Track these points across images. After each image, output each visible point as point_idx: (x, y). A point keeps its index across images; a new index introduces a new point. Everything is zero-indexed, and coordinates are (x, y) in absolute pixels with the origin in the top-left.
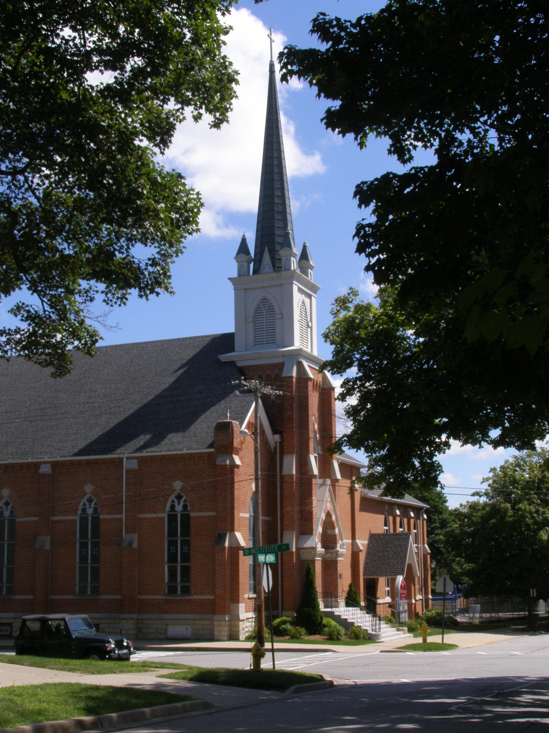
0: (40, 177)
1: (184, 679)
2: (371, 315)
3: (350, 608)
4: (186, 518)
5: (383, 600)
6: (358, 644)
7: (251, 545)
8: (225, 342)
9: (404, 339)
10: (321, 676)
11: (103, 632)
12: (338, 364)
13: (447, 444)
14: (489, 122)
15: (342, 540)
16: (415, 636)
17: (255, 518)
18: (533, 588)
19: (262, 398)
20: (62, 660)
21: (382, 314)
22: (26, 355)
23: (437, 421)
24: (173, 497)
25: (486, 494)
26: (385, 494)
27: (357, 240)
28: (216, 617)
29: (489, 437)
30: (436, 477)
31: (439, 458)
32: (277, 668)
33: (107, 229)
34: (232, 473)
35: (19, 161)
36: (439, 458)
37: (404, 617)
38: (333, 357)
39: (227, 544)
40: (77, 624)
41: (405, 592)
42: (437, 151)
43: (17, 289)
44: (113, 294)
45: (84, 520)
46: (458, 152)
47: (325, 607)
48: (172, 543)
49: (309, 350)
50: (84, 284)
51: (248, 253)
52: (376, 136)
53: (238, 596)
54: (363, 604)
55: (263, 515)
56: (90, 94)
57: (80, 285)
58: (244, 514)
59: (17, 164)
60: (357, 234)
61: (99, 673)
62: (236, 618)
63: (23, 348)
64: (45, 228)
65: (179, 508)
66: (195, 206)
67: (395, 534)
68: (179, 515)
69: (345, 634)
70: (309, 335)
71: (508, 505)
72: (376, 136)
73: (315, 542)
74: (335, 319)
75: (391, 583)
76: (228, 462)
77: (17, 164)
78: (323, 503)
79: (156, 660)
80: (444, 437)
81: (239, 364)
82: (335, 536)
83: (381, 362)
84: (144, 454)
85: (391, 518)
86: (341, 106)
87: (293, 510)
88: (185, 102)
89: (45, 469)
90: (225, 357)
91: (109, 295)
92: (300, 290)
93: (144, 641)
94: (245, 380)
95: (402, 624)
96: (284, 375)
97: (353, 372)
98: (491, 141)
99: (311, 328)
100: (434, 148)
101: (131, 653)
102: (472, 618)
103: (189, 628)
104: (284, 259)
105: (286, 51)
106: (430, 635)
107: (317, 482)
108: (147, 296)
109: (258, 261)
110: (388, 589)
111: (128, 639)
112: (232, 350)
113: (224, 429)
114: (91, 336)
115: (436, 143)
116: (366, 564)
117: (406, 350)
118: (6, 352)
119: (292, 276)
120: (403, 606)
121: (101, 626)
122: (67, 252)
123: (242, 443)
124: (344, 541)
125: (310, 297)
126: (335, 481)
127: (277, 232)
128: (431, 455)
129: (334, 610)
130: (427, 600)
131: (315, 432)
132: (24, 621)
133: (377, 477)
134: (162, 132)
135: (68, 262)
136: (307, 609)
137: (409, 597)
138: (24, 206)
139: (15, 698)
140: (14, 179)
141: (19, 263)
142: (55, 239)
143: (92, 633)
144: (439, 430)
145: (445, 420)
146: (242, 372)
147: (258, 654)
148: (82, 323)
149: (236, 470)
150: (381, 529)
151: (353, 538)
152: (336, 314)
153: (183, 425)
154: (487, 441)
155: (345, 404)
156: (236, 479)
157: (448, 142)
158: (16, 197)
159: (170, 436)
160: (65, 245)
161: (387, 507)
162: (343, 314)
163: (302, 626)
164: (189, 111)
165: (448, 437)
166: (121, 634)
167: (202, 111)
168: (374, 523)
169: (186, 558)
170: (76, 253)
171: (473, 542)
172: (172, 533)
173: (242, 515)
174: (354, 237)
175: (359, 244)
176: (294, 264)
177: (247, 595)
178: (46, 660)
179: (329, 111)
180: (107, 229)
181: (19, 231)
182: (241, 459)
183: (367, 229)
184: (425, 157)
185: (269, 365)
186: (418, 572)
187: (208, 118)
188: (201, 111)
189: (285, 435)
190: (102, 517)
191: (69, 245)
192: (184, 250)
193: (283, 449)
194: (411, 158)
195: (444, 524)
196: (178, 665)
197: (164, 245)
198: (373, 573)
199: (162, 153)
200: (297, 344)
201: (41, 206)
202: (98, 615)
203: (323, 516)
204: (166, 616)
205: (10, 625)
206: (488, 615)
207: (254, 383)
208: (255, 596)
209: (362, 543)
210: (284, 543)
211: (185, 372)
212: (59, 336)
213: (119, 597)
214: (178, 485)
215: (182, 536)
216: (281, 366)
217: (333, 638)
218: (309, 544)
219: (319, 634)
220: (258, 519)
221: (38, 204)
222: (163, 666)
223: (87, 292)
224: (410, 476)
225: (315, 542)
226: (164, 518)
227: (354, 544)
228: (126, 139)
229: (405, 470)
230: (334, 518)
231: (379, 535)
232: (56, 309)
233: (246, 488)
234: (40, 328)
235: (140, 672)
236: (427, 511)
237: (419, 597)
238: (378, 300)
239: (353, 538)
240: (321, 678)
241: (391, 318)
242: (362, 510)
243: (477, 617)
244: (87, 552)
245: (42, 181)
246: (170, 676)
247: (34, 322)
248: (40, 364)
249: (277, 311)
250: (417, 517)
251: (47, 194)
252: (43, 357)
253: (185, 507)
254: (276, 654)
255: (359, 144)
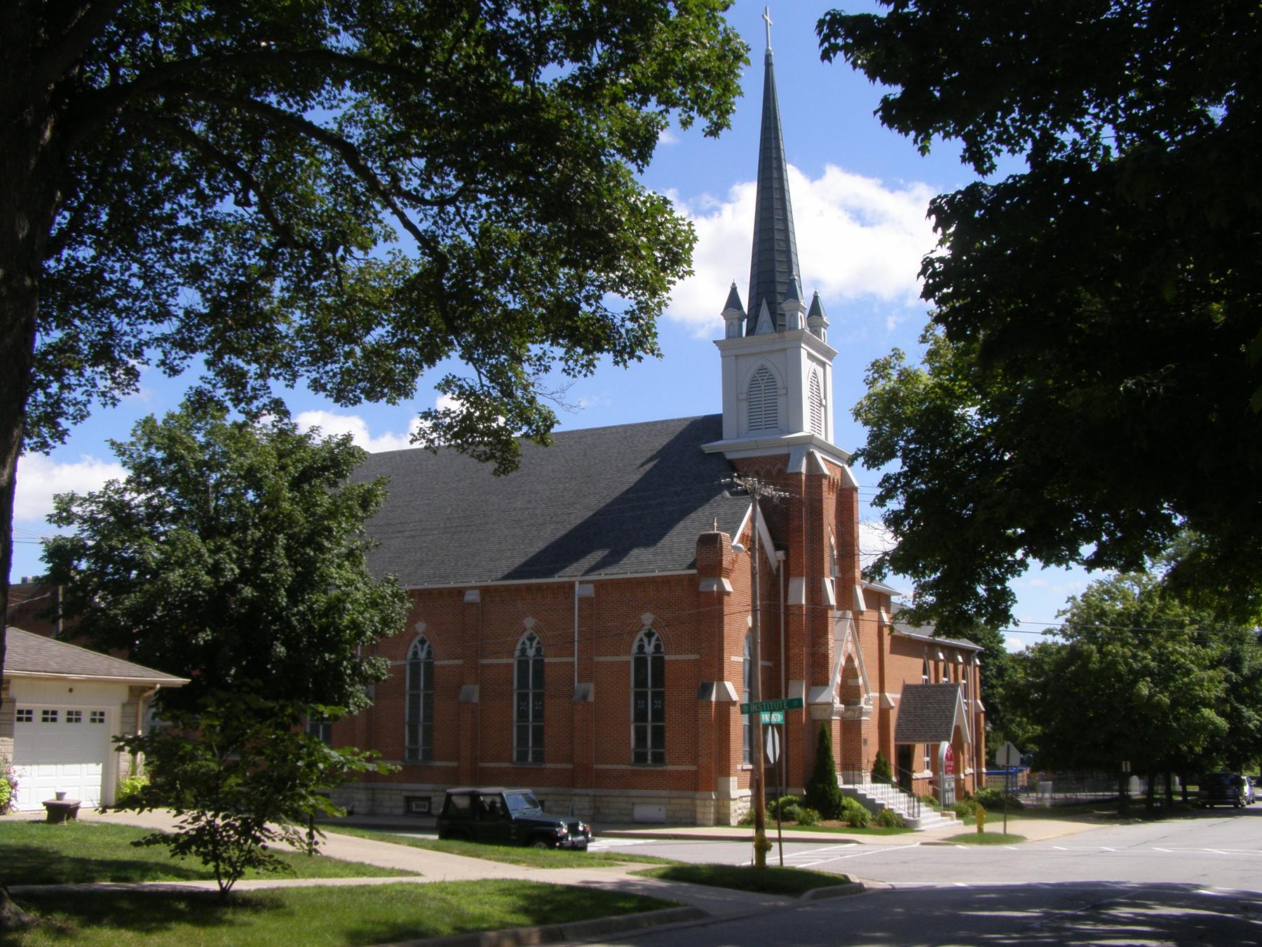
0: (476, 206)
1: (652, 876)
2: (922, 387)
3: (879, 785)
4: (659, 662)
5: (922, 773)
6: (891, 834)
7: (746, 701)
8: (709, 426)
9: (962, 418)
10: (846, 877)
11: (549, 812)
12: (874, 457)
13: (1023, 564)
14: (1101, 115)
15: (867, 692)
16: (966, 823)
17: (752, 663)
18: (1126, 760)
19: (760, 502)
20: (502, 848)
21: (935, 386)
22: (458, 446)
23: (1010, 531)
24: (641, 635)
25: (1063, 632)
26: (936, 633)
27: (922, 280)
28: (699, 794)
29: (1079, 554)
30: (1006, 610)
31: (1012, 583)
32: (786, 864)
33: (564, 274)
34: (721, 602)
35: (449, 186)
36: (1012, 583)
37: (951, 797)
38: (870, 443)
39: (713, 698)
40: (518, 801)
41: (952, 763)
42: (1029, 158)
43: (444, 358)
44: (576, 361)
45: (523, 664)
46: (1058, 157)
47: (845, 783)
48: (640, 696)
49: (823, 438)
50: (535, 349)
51: (740, 307)
52: (944, 138)
53: (729, 767)
54: (894, 779)
55: (763, 659)
56: (543, 95)
57: (529, 350)
58: (736, 658)
59: (445, 191)
60: (923, 272)
61: (551, 866)
62: (725, 797)
63: (455, 436)
64: (482, 275)
65: (649, 649)
66: (687, 239)
67: (938, 686)
68: (649, 659)
69: (872, 820)
70: (828, 413)
71: (1093, 647)
72: (944, 138)
73: (832, 695)
74: (871, 391)
75: (933, 751)
76: (715, 588)
77: (445, 191)
78: (843, 643)
79: (615, 850)
80: (1019, 554)
81: (729, 456)
82: (858, 687)
83: (933, 452)
84: (603, 575)
85: (932, 663)
86: (903, 93)
87: (802, 653)
88: (669, 102)
89: (473, 596)
90: (708, 447)
91: (571, 362)
92: (810, 356)
93: (604, 823)
94: (739, 477)
95: (947, 807)
96: (789, 471)
97: (895, 466)
98: (1105, 142)
99: (825, 407)
100: (1025, 153)
101: (588, 841)
102: (1041, 799)
103: (663, 809)
104: (788, 314)
105: (828, 18)
106: (987, 821)
107: (833, 614)
108: (625, 362)
109: (753, 317)
110: (927, 759)
111: (584, 822)
112: (719, 437)
113: (710, 543)
114: (545, 419)
115: (1028, 146)
116: (899, 725)
117: (965, 436)
118: (432, 441)
119: (800, 337)
120: (949, 782)
121: (546, 804)
122: (511, 306)
123: (734, 562)
124: (871, 694)
125: (823, 365)
126: (858, 614)
127: (779, 278)
128: (1002, 581)
129: (857, 786)
130: (979, 774)
131: (831, 547)
132: (449, 796)
133: (926, 610)
134: (640, 144)
135: (514, 319)
136: (821, 786)
137: (956, 770)
138: (454, 247)
139: (449, 897)
140: (442, 211)
141: (449, 321)
142: (496, 289)
143: (536, 813)
144: (1012, 545)
145: (1019, 531)
146: (732, 466)
147: (762, 847)
148: (532, 401)
149: (726, 598)
150: (918, 678)
151: (882, 690)
152: (872, 383)
153: (651, 538)
154: (1076, 561)
155: (885, 509)
156: (726, 610)
157: (1046, 143)
158: (444, 235)
159: (635, 552)
160: (510, 297)
161: (926, 649)
162: (881, 385)
163: (815, 808)
164: (675, 114)
165: (1026, 555)
166: (573, 815)
167: (694, 114)
168: (909, 670)
169: (659, 715)
170: (524, 307)
171: (1044, 697)
172: (641, 682)
173: (734, 658)
174: (919, 276)
175: (927, 286)
176: (802, 323)
177: (741, 766)
178: (483, 847)
179: (885, 100)
180: (564, 274)
181: (449, 280)
182: (732, 583)
183: (937, 265)
184: (1011, 165)
185: (769, 457)
186: (968, 736)
187: (701, 123)
188: (692, 114)
189: (791, 551)
190: (547, 660)
191: (515, 296)
192: (668, 302)
193: (788, 570)
194: (993, 167)
195: (1001, 671)
196: (653, 858)
197: (643, 294)
198: (907, 738)
199: (641, 171)
200: (807, 429)
201: (477, 246)
202: (543, 790)
203: (843, 661)
204: (633, 792)
205: (428, 799)
206: (1061, 795)
207: (751, 482)
208: (750, 767)
209: (893, 697)
210: (790, 697)
211: (655, 466)
212: (502, 420)
213: (570, 766)
214: (647, 618)
215: (653, 686)
216: (785, 459)
217: (856, 824)
218: (822, 698)
219: (837, 818)
220: (756, 664)
221: (473, 244)
222: (632, 858)
223: (539, 359)
224: (970, 609)
225: (832, 695)
226: (512, 665)
227: (882, 699)
228: (592, 155)
229: (965, 600)
230: (856, 663)
231: (916, 687)
232: (498, 384)
233: (739, 623)
234: (477, 409)
235: (603, 865)
236: (981, 655)
237: (969, 770)
238: (927, 367)
239: (882, 690)
240: (845, 880)
241: (948, 392)
242: (892, 652)
243: (1047, 797)
244: (534, 706)
245: (479, 212)
246: (1069, 929)
247: (468, 401)
248: (479, 457)
249: (780, 385)
250: (967, 661)
251: (485, 232)
252: (482, 448)
253: (657, 647)
254: (784, 844)
255: (920, 149)
